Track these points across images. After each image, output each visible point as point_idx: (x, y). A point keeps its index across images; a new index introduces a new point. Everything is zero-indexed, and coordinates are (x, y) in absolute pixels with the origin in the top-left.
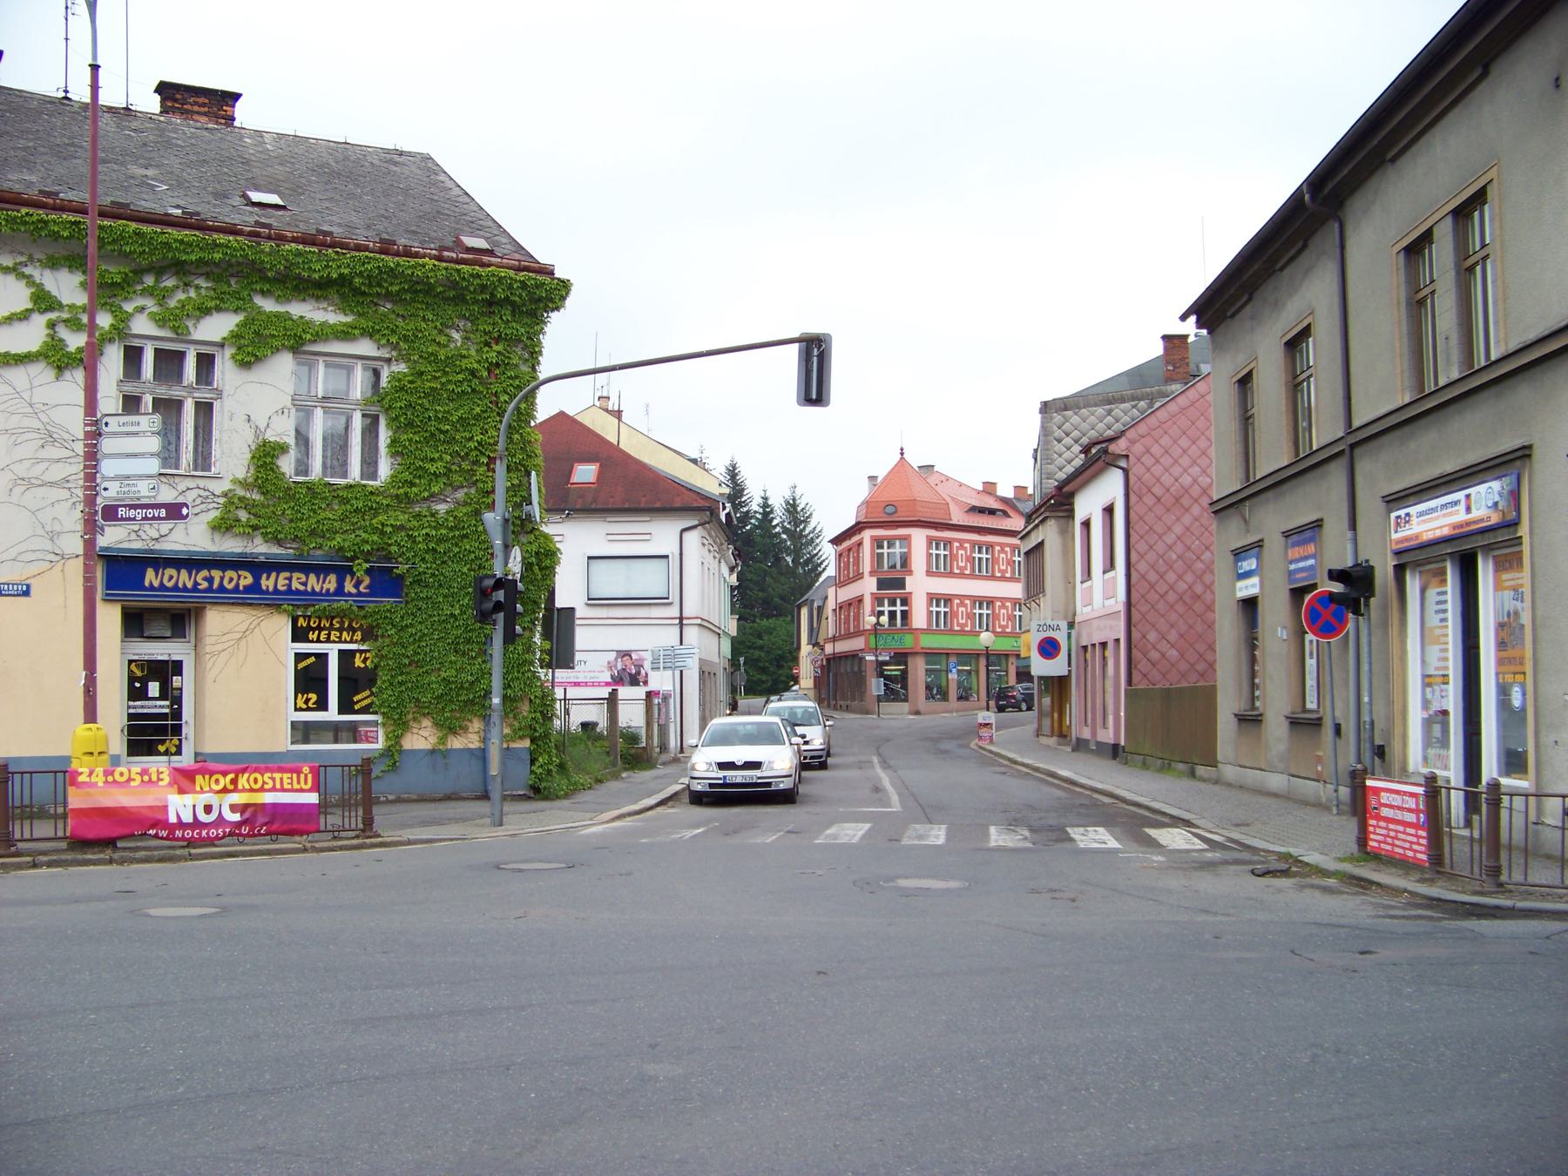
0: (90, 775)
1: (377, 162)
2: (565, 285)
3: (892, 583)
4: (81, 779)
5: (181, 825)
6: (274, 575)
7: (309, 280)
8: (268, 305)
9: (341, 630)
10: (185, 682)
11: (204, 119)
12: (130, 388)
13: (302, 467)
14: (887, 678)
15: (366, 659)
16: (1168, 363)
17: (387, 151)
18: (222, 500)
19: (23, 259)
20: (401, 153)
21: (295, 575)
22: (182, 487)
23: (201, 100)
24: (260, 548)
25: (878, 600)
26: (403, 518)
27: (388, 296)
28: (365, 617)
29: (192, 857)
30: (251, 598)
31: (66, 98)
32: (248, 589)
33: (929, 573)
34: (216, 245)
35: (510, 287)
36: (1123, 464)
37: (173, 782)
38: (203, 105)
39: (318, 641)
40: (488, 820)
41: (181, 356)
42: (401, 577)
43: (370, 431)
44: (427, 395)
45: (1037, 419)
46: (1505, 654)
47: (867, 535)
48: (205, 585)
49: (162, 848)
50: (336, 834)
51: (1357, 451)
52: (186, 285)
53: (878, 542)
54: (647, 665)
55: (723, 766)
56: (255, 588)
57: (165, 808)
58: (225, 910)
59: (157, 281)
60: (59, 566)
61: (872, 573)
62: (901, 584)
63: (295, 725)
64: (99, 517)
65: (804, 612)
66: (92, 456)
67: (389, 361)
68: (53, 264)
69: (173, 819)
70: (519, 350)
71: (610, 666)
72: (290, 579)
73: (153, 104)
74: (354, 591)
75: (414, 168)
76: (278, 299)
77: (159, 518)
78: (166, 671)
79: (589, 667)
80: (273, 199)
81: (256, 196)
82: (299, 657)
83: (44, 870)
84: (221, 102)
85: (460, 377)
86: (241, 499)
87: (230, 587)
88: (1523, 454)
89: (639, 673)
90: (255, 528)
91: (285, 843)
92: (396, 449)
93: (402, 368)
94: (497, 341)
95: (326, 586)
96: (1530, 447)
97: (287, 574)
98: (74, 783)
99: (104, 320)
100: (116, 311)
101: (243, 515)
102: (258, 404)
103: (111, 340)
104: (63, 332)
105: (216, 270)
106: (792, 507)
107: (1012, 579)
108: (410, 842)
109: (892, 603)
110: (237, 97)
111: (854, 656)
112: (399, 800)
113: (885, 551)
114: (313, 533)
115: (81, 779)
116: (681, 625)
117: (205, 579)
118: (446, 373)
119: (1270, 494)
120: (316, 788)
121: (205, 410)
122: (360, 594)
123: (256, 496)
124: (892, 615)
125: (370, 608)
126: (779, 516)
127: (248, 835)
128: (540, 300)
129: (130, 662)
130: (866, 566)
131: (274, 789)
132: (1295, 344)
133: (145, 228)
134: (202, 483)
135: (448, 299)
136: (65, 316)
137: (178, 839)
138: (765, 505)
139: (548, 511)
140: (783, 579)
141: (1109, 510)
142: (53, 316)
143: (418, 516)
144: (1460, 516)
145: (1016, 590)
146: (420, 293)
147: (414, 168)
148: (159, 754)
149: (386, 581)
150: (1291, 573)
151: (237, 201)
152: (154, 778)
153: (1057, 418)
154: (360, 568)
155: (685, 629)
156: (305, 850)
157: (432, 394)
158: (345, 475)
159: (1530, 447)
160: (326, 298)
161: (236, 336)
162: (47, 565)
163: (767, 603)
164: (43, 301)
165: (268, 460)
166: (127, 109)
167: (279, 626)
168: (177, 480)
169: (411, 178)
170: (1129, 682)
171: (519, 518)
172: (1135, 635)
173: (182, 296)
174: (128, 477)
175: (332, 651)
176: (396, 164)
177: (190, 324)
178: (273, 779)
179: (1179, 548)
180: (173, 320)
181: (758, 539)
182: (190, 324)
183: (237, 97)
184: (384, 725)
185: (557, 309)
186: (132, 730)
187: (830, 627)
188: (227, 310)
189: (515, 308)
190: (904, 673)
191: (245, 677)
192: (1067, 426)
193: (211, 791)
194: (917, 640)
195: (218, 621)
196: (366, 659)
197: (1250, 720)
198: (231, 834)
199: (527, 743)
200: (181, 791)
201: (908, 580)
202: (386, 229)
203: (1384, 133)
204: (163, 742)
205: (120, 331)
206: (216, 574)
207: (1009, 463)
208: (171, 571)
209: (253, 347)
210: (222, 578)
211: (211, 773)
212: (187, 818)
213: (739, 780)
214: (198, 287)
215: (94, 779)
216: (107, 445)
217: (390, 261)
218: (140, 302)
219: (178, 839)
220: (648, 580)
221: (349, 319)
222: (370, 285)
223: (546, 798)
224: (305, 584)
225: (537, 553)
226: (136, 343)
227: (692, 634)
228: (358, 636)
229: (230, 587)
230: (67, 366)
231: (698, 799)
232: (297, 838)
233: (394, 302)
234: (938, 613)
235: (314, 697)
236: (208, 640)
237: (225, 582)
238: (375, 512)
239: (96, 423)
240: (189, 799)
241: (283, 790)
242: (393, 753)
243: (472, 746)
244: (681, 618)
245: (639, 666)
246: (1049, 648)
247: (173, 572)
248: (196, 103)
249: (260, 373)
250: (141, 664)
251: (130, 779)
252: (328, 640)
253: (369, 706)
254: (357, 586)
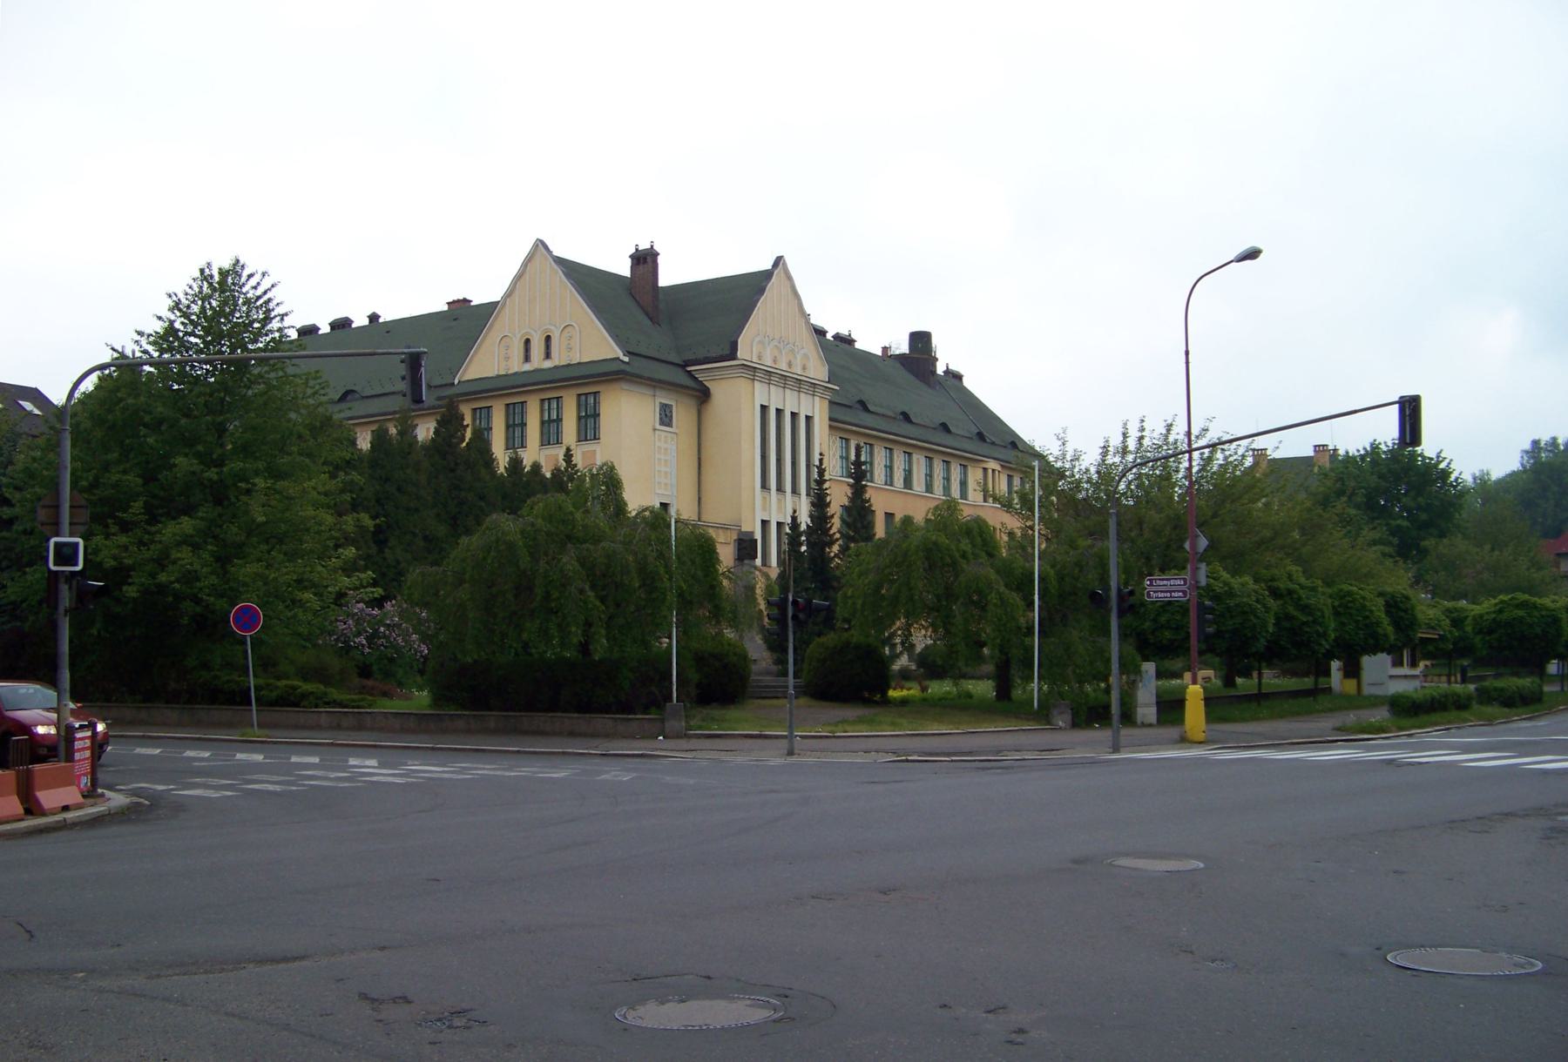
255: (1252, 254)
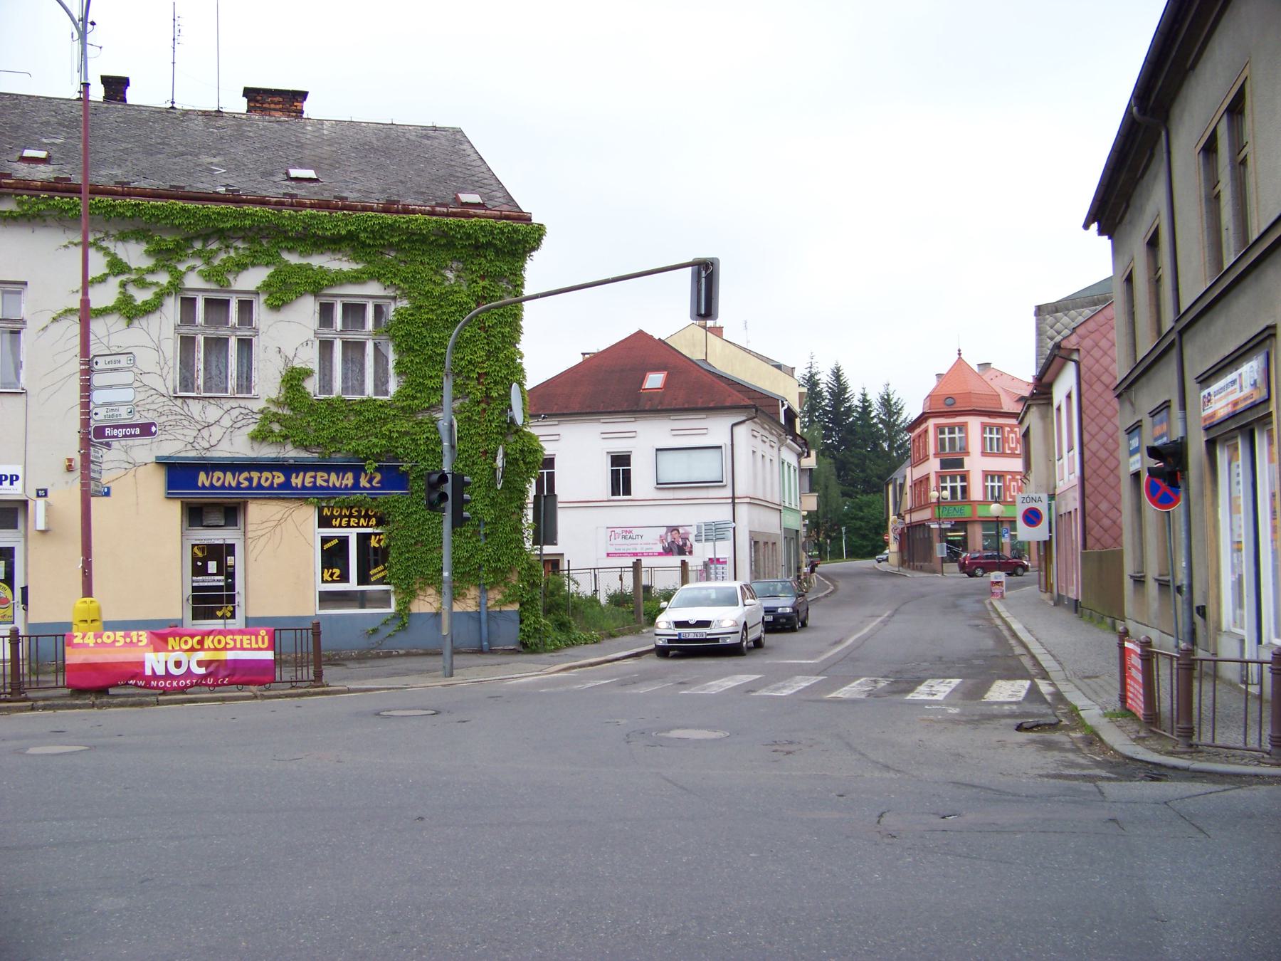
0: (84, 637)
1: (412, 138)
2: (540, 231)
3: (952, 463)
4: (76, 641)
5: (155, 676)
6: (301, 474)
7: (324, 237)
8: (293, 259)
9: (359, 517)
10: (236, 561)
11: (278, 114)
12: (186, 331)
13: (326, 385)
14: (949, 542)
15: (379, 541)
17: (424, 128)
18: (259, 416)
19: (101, 235)
20: (435, 129)
21: (319, 474)
22: (227, 407)
23: (277, 99)
24: (291, 453)
25: (942, 478)
26: (406, 426)
27: (391, 246)
28: (378, 507)
29: (158, 703)
30: (285, 493)
31: (172, 108)
32: (280, 486)
33: (984, 454)
34: (245, 215)
35: (492, 233)
36: (1075, 357)
37: (151, 642)
38: (279, 103)
39: (340, 526)
40: (441, 673)
41: (227, 302)
42: (406, 473)
43: (380, 357)
44: (424, 325)
45: (1032, 320)
47: (931, 423)
48: (246, 484)
49: (139, 695)
50: (294, 683)
51: (1185, 337)
52: (227, 247)
53: (940, 429)
54: (692, 538)
55: (679, 624)
56: (286, 485)
57: (142, 664)
58: (93, 748)
59: (204, 246)
60: (132, 472)
61: (936, 455)
62: (960, 463)
64: (92, 436)
65: (891, 488)
66: (87, 388)
67: (394, 298)
68: (123, 237)
69: (148, 672)
70: (503, 284)
71: (662, 539)
72: (315, 477)
73: (239, 105)
74: (368, 485)
75: (443, 141)
76: (301, 254)
77: (135, 435)
78: (221, 553)
79: (645, 540)
80: (310, 174)
81: (294, 173)
82: (325, 540)
83: (40, 712)
84: (292, 100)
85: (453, 309)
86: (275, 414)
87: (266, 485)
89: (685, 544)
90: (286, 437)
91: (233, 692)
92: (401, 369)
93: (405, 303)
94: (483, 277)
95: (345, 482)
96: (1273, 327)
97: (313, 474)
98: (71, 644)
99: (164, 279)
100: (173, 271)
101: (276, 427)
102: (288, 338)
103: (169, 294)
104: (132, 290)
105: (250, 234)
106: (886, 402)
107: (1013, 455)
108: (349, 691)
109: (953, 479)
110: (303, 95)
111: (921, 525)
112: (408, 655)
113: (947, 436)
114: (333, 439)
115: (76, 641)
116: (734, 503)
117: (246, 479)
118: (441, 306)
119: (1144, 380)
120: (272, 646)
121: (245, 344)
122: (373, 488)
123: (287, 412)
124: (953, 489)
125: (381, 499)
126: (876, 409)
127: (212, 685)
128: (519, 241)
129: (193, 546)
130: (931, 449)
131: (234, 648)
132: (1153, 243)
133: (190, 205)
134: (243, 403)
135: (447, 243)
136: (133, 277)
137: (153, 688)
138: (864, 400)
139: (532, 416)
140: (880, 461)
141: (1069, 397)
142: (124, 278)
143: (420, 424)
145: (1016, 465)
146: (416, 241)
147: (443, 141)
148: (217, 618)
149: (394, 478)
151: (280, 177)
152: (135, 640)
153: (1050, 319)
154: (371, 466)
155: (737, 507)
156: (255, 697)
157: (428, 324)
158: (362, 393)
159: (1273, 327)
160: (339, 251)
161: (267, 285)
162: (123, 472)
163: (866, 481)
164: (117, 267)
165: (295, 383)
166: (218, 111)
167: (307, 516)
168: (223, 401)
169: (445, 150)
170: (1085, 546)
171: (505, 422)
172: (1089, 505)
173: (224, 256)
174: (111, 404)
175: (352, 534)
176: (428, 137)
177: (231, 278)
178: (235, 641)
180: (217, 275)
181: (859, 429)
182: (231, 278)
183: (303, 95)
184: (395, 592)
185: (534, 249)
186: (196, 599)
187: (908, 502)
188: (259, 265)
189: (498, 252)
190: (965, 537)
191: (283, 558)
192: (1058, 326)
193: (181, 650)
194: (974, 511)
195: (257, 512)
196: (379, 541)
197: (1139, 581)
198: (197, 684)
199: (516, 607)
200: (156, 650)
201: (966, 460)
202: (395, 192)
203: (1178, 42)
204: (221, 609)
205: (176, 287)
206: (255, 475)
207: (1019, 363)
208: (218, 474)
209: (281, 293)
210: (260, 478)
211: (181, 636)
212: (161, 671)
213: (691, 637)
214: (236, 248)
215: (86, 641)
216: (97, 380)
217: (389, 218)
218: (191, 262)
219: (153, 688)
220: (705, 467)
221: (360, 267)
222: (375, 239)
223: (534, 652)
224: (327, 481)
225: (522, 451)
226: (190, 295)
227: (742, 510)
228: (373, 521)
229: (266, 485)
230: (135, 316)
231: (662, 652)
232: (252, 688)
233: (397, 251)
234: (993, 487)
235: (337, 572)
236: (250, 528)
237: (263, 482)
238: (385, 421)
239: (88, 363)
240: (162, 656)
241: (242, 649)
242: (403, 618)
243: (469, 610)
244: (733, 498)
245: (685, 539)
246: (1032, 517)
247: (221, 474)
248: (273, 102)
249: (289, 314)
250: (202, 547)
251: (115, 641)
252: (348, 526)
253: (384, 578)
254: (370, 481)
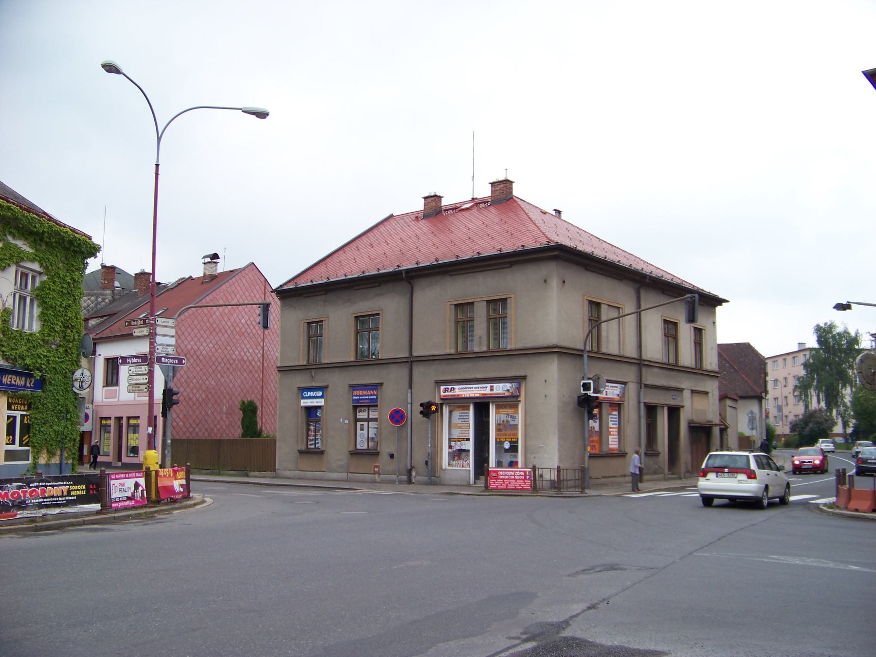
16: (105, 280)
34: (9, 208)
46: (513, 432)
63: (7, 452)
67: (40, 273)
82: (9, 417)
88: (524, 378)
144: (488, 391)
150: (354, 400)
179: (185, 377)
255: (262, 115)
